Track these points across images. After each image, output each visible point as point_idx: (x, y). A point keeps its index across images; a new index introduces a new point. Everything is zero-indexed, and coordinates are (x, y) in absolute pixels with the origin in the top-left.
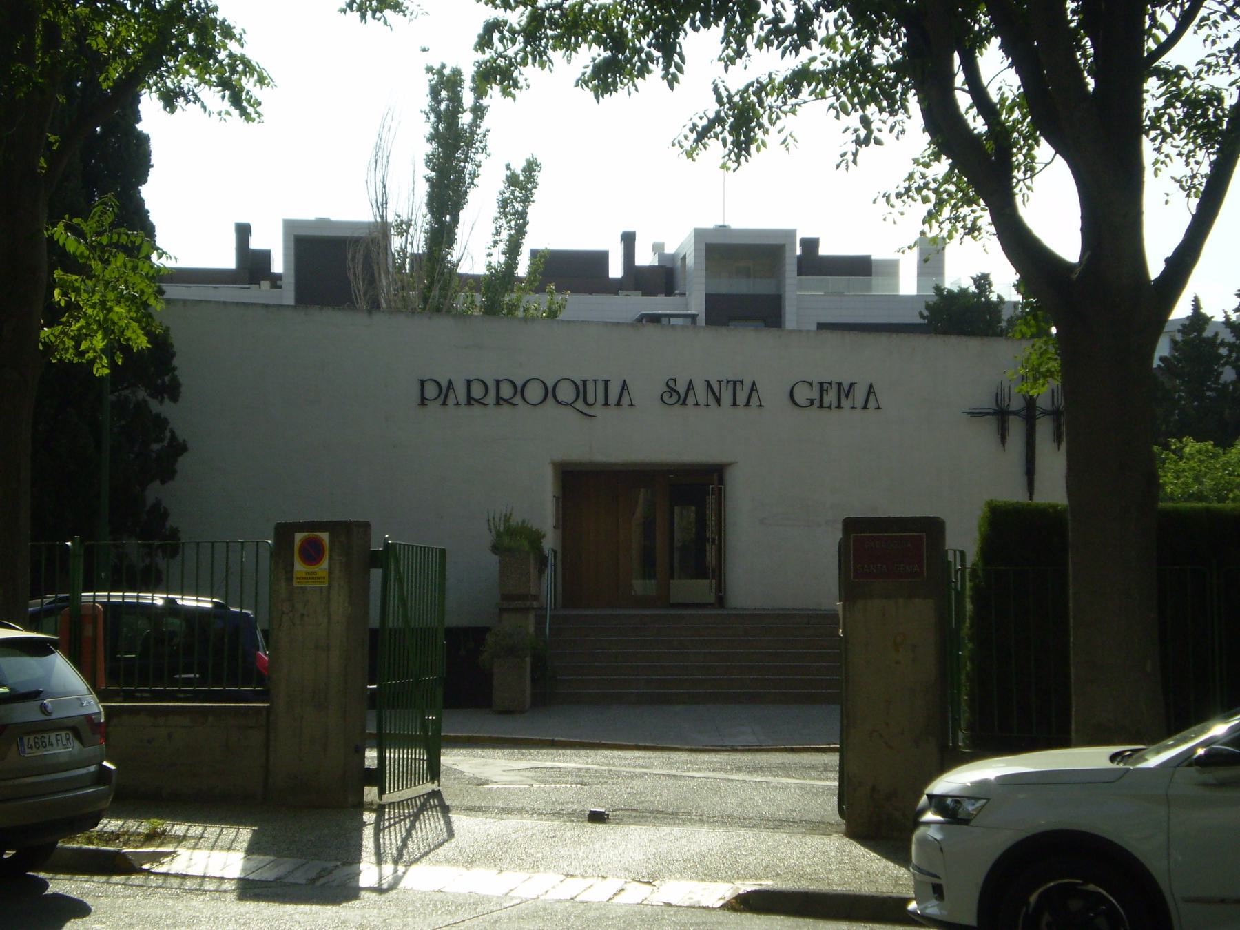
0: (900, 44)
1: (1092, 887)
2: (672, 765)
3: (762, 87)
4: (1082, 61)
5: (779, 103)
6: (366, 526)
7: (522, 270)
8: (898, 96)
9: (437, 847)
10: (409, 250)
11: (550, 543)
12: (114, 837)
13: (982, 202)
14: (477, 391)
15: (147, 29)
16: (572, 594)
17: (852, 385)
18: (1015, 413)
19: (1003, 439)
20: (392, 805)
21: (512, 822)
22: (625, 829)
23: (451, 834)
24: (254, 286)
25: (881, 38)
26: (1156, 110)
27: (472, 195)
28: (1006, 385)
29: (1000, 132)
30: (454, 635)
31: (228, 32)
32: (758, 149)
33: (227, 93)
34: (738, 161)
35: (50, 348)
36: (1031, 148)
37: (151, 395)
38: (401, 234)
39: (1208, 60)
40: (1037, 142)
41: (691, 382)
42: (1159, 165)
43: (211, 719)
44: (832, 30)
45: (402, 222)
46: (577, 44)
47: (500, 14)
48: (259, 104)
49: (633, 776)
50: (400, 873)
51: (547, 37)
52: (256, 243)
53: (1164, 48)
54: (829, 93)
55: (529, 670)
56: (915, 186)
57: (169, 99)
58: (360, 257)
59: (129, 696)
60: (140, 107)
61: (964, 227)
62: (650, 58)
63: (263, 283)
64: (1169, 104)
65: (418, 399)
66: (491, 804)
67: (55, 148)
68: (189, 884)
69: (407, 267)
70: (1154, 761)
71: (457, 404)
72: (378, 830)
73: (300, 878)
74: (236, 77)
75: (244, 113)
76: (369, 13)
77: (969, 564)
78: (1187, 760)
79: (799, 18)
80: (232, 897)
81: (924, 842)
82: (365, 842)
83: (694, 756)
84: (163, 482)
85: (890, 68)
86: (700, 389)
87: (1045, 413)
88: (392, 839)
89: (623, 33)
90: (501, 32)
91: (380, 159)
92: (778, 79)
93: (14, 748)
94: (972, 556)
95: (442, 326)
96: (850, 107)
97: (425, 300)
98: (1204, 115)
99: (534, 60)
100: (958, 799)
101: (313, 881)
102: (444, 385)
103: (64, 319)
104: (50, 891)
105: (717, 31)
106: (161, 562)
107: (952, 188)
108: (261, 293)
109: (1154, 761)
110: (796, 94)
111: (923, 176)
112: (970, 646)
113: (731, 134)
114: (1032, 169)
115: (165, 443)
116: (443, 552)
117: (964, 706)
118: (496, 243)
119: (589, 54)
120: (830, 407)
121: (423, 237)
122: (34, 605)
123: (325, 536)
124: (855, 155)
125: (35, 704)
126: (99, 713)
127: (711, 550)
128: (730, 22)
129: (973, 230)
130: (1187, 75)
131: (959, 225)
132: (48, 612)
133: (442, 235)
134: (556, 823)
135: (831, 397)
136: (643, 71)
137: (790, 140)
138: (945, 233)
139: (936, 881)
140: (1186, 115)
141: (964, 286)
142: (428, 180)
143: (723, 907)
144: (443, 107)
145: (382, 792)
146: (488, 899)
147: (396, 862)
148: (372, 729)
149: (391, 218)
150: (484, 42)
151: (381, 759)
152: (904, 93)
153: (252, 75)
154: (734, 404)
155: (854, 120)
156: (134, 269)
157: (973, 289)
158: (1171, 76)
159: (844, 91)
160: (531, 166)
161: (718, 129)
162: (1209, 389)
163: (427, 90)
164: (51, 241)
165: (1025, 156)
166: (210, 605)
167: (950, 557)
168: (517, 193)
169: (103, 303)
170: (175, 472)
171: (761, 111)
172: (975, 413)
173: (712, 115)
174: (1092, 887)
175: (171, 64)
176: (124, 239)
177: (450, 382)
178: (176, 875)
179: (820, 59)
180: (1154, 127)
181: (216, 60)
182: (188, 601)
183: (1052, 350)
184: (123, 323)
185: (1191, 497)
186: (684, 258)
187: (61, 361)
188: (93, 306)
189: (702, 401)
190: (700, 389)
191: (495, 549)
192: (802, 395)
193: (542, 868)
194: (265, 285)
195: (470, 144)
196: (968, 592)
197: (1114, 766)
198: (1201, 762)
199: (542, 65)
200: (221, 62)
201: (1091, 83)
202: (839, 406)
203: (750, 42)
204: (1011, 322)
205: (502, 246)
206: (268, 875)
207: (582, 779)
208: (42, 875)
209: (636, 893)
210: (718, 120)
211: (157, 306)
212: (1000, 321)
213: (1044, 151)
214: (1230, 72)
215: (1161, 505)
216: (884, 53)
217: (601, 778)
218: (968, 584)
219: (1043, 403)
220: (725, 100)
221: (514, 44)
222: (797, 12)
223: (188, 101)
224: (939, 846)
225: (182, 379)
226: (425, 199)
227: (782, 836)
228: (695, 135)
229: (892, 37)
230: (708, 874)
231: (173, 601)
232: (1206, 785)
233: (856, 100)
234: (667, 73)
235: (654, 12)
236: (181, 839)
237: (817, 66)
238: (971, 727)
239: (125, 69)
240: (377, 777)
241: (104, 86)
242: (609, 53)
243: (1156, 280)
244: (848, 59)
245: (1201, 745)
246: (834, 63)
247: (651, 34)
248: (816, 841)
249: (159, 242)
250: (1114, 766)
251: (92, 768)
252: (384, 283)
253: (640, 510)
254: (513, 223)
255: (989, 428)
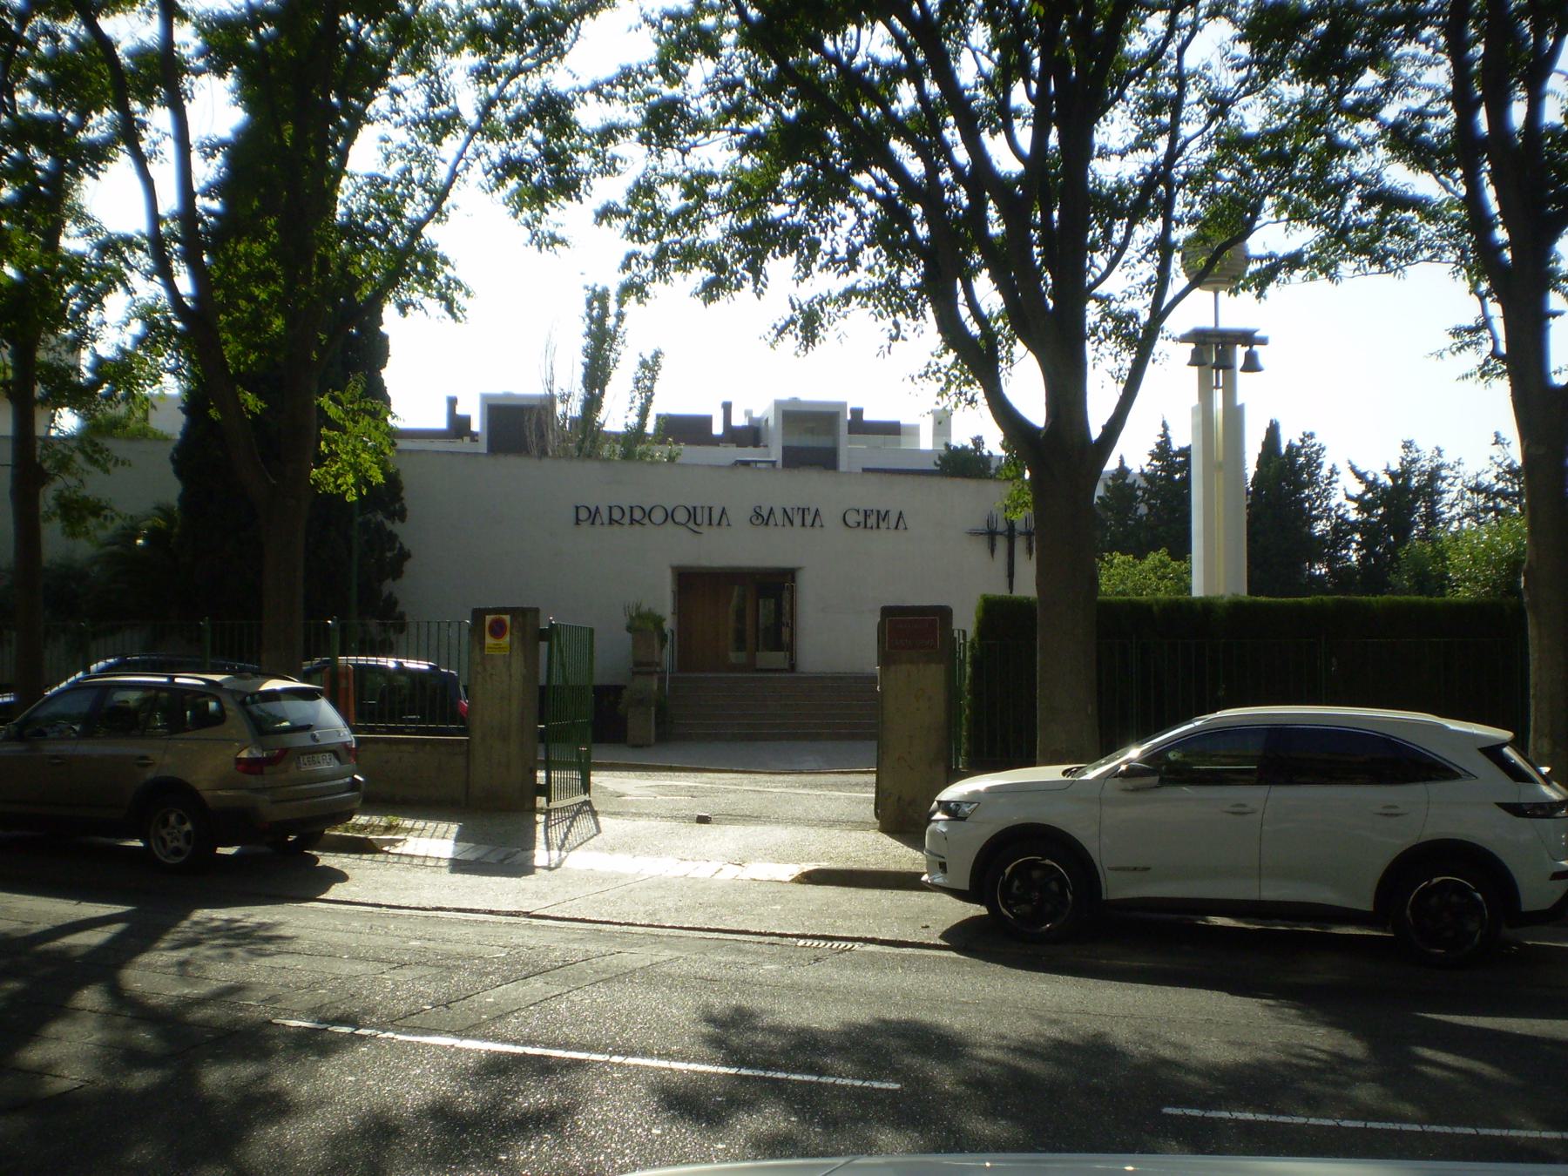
0: (920, 271)
1: (1048, 862)
2: (757, 783)
3: (823, 299)
4: (1044, 288)
5: (835, 310)
6: (537, 611)
7: (650, 428)
8: (919, 307)
9: (589, 839)
10: (569, 414)
11: (669, 624)
12: (363, 828)
13: (978, 383)
14: (617, 515)
15: (390, 260)
16: (685, 661)
17: (887, 512)
18: (1001, 534)
19: (992, 551)
20: (556, 810)
21: (642, 823)
22: (723, 827)
23: (599, 831)
24: (460, 441)
25: (906, 267)
26: (1095, 323)
27: (615, 375)
28: (994, 513)
29: (989, 335)
30: (601, 691)
31: (445, 261)
32: (820, 342)
33: (444, 303)
34: (806, 350)
35: (318, 484)
36: (1011, 346)
37: (387, 518)
38: (563, 402)
39: (1129, 290)
40: (1015, 343)
41: (772, 509)
42: (1096, 361)
43: (428, 747)
44: (872, 261)
45: (564, 394)
46: (691, 267)
47: (637, 247)
48: (465, 310)
49: (729, 792)
50: (563, 856)
51: (669, 262)
52: (461, 410)
53: (1098, 282)
54: (870, 304)
55: (653, 716)
56: (931, 370)
57: (403, 308)
58: (534, 418)
59: (372, 730)
60: (383, 315)
61: (966, 400)
62: (744, 277)
63: (465, 438)
64: (1103, 319)
65: (573, 518)
66: (626, 810)
67: (323, 343)
68: (415, 861)
69: (567, 426)
70: (1092, 774)
71: (602, 524)
72: (547, 827)
73: (492, 859)
74: (450, 291)
75: (454, 316)
76: (544, 247)
77: (968, 639)
78: (1114, 774)
79: (849, 252)
80: (446, 871)
81: (934, 833)
82: (537, 835)
83: (773, 777)
84: (394, 580)
85: (913, 288)
86: (779, 514)
87: (1021, 534)
88: (557, 833)
89: (724, 260)
90: (637, 259)
91: (549, 350)
92: (834, 294)
93: (294, 764)
94: (971, 633)
95: (592, 467)
96: (885, 314)
97: (580, 449)
98: (1127, 327)
99: (660, 278)
100: (958, 804)
101: (502, 861)
102: (593, 511)
103: (327, 463)
104: (320, 864)
105: (791, 259)
106: (393, 636)
107: (957, 373)
108: (464, 445)
109: (1092, 774)
110: (848, 303)
111: (937, 364)
112: (969, 697)
113: (801, 331)
114: (1012, 361)
115: (396, 552)
116: (592, 631)
117: (963, 740)
118: (631, 409)
119: (700, 274)
120: (872, 528)
121: (579, 404)
122: (306, 666)
123: (507, 618)
124: (889, 347)
125: (307, 734)
126: (351, 742)
127: (786, 631)
128: (800, 254)
129: (972, 401)
130: (1114, 299)
131: (962, 398)
132: (316, 670)
133: (592, 404)
134: (674, 823)
135: (872, 521)
136: (739, 286)
137: (843, 337)
138: (953, 404)
139: (942, 860)
140: (1114, 328)
141: (965, 444)
142: (583, 364)
143: (793, 881)
144: (595, 313)
145: (549, 801)
146: (626, 876)
147: (560, 849)
148: (541, 757)
149: (556, 392)
150: (626, 266)
151: (548, 778)
152: (923, 305)
153: (461, 290)
154: (803, 525)
155: (888, 323)
156: (377, 428)
157: (971, 446)
158: (1102, 300)
159: (880, 303)
160: (657, 355)
161: (792, 327)
162: (1130, 519)
163: (584, 301)
164: (321, 410)
165: (1007, 352)
166: (426, 667)
167: (956, 634)
168: (646, 373)
169: (354, 451)
170: (402, 572)
171: (822, 315)
172: (974, 533)
173: (788, 318)
174: (1048, 862)
175: (405, 283)
176: (369, 406)
177: (597, 508)
178: (407, 855)
179: (864, 281)
180: (1094, 334)
181: (436, 280)
182: (411, 664)
183: (1026, 488)
184: (367, 465)
185: (1118, 593)
186: (767, 420)
187: (325, 492)
188: (347, 453)
189: (780, 522)
190: (779, 514)
191: (629, 629)
192: (852, 518)
193: (663, 855)
194: (467, 439)
195: (613, 339)
196: (968, 659)
197: (1065, 778)
198: (1123, 775)
199: (666, 282)
200: (439, 282)
201: (1051, 303)
202: (878, 527)
203: (815, 267)
204: (998, 469)
205: (636, 411)
206: (470, 856)
207: (692, 793)
208: (315, 853)
209: (730, 872)
210: (793, 321)
211: (391, 454)
212: (989, 468)
213: (1020, 348)
214: (1143, 298)
215: (1099, 598)
216: (910, 277)
217: (705, 793)
218: (968, 654)
219: (1020, 526)
220: (797, 307)
221: (646, 267)
222: (848, 248)
223: (415, 308)
224: (945, 836)
225: (407, 506)
226: (581, 378)
227: (835, 832)
228: (775, 332)
229: (914, 267)
230: (783, 859)
231: (401, 664)
232: (1126, 790)
233: (889, 309)
234: (756, 288)
235: (746, 246)
236: (409, 831)
237: (861, 286)
238: (968, 754)
239: (373, 288)
240: (545, 791)
241: (358, 299)
242: (714, 274)
243: (1096, 441)
244: (883, 281)
245: (1125, 762)
246: (874, 284)
247: (744, 261)
248: (858, 835)
249: (393, 409)
250: (1065, 778)
251: (348, 780)
252: (551, 437)
253: (734, 602)
254: (643, 395)
255: (981, 545)
